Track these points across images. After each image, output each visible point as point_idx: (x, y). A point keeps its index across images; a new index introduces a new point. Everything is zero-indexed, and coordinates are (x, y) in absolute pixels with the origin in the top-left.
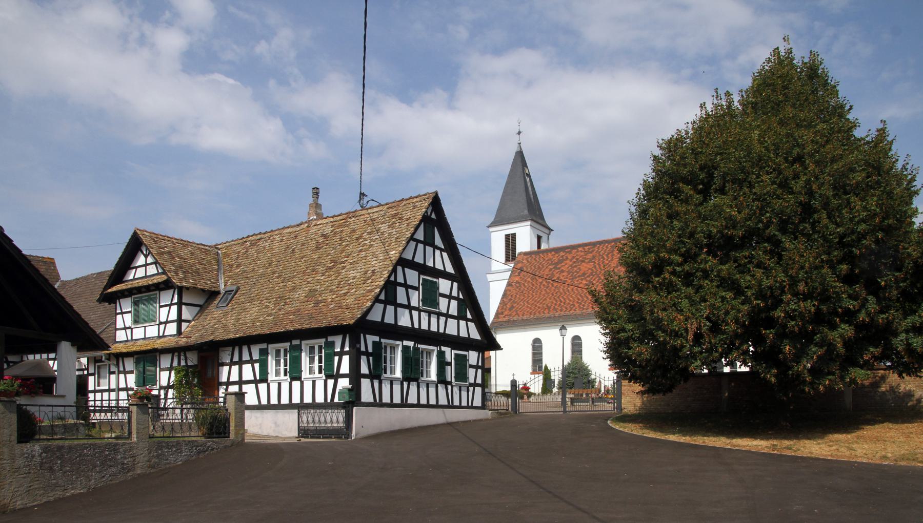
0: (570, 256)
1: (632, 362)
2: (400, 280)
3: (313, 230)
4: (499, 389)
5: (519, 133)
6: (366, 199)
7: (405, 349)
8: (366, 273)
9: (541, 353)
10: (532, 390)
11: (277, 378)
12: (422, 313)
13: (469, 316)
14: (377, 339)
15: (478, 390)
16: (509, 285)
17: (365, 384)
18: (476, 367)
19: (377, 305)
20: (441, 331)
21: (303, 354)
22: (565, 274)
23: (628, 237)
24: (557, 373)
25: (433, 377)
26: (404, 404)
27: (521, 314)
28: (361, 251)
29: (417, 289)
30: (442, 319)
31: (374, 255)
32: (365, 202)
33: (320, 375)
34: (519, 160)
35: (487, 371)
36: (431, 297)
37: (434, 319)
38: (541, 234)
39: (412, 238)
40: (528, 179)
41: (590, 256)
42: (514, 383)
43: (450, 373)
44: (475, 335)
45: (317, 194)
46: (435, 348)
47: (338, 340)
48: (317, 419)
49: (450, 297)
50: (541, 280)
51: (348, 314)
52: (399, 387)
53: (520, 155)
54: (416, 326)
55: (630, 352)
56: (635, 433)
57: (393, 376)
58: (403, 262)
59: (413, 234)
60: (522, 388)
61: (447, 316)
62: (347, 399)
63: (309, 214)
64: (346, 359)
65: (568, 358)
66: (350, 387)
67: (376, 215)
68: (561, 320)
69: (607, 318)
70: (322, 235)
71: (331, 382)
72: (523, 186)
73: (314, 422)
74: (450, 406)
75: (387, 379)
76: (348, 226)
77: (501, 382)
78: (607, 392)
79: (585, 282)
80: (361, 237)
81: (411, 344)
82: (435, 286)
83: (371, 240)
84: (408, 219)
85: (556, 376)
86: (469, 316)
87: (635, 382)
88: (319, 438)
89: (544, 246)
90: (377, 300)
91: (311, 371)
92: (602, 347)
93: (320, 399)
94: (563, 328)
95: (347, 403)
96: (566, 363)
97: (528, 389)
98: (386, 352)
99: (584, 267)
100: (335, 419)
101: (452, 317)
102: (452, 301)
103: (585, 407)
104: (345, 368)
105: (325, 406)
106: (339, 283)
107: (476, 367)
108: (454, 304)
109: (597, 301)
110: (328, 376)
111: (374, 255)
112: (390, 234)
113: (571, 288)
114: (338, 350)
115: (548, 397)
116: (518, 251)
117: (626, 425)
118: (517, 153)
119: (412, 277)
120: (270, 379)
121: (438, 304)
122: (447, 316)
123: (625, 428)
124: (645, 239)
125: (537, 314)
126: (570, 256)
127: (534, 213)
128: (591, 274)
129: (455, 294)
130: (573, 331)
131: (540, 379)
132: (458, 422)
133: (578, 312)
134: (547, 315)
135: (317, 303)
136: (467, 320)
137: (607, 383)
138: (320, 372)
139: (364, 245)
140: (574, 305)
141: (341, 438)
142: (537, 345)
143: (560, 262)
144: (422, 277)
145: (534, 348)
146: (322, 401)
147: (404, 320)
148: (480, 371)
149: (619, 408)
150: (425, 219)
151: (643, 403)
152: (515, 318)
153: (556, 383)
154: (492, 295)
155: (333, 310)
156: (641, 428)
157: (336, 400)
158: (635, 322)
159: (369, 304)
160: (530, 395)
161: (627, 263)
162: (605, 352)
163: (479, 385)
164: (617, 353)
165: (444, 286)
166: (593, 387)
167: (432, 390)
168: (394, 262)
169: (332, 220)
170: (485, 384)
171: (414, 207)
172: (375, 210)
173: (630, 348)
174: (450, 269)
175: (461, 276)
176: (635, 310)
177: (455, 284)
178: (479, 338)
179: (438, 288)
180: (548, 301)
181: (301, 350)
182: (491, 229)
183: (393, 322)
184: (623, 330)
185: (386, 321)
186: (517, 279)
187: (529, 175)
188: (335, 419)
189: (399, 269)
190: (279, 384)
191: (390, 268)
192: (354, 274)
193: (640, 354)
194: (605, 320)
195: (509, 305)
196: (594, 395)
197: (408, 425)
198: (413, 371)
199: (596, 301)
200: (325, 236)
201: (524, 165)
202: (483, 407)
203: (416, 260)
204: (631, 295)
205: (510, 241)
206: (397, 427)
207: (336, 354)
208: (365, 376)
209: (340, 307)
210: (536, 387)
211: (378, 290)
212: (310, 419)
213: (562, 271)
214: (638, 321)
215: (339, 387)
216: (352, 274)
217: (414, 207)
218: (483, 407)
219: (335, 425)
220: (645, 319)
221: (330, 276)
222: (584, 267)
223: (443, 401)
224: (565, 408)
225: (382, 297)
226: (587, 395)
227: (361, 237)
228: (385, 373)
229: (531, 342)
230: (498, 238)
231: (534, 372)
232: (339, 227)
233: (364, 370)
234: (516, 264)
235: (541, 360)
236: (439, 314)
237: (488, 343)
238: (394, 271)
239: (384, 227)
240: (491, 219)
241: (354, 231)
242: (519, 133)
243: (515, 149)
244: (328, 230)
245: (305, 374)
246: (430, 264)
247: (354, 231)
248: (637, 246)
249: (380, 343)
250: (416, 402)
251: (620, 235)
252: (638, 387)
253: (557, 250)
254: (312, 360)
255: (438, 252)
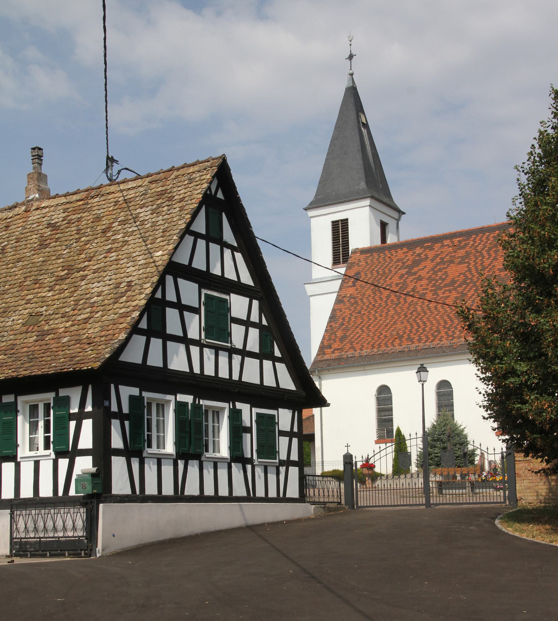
0: (431, 254)
1: (529, 424)
2: (171, 296)
3: (35, 216)
4: (328, 468)
5: (351, 57)
6: (116, 168)
7: (180, 407)
8: (118, 286)
9: (391, 410)
10: (377, 470)
11: (33, 453)
12: (206, 350)
13: (277, 353)
14: (135, 391)
15: (294, 471)
16: (339, 301)
17: (118, 465)
18: (290, 434)
19: (135, 337)
20: (235, 377)
21: (20, 418)
23: (516, 222)
24: (414, 442)
25: (224, 452)
26: (179, 497)
27: (358, 347)
28: (109, 251)
29: (196, 311)
30: (237, 359)
31: (129, 257)
32: (115, 172)
33: (47, 452)
34: (352, 100)
35: (306, 440)
36: (218, 323)
37: (223, 359)
38: (386, 219)
39: (188, 231)
40: (364, 131)
41: (461, 253)
42: (348, 459)
43: (250, 444)
44: (287, 383)
45: (40, 157)
46: (225, 405)
47: (74, 395)
48: (41, 524)
49: (247, 323)
50: (388, 292)
51: (90, 352)
52: (171, 468)
53: (352, 93)
54: (197, 370)
55: (525, 408)
56: (538, 540)
57: (162, 451)
58: (175, 269)
59: (189, 224)
60: (363, 466)
61: (244, 353)
62: (89, 490)
63: (27, 190)
64: (87, 425)
65: (431, 418)
66: (94, 470)
67: (131, 194)
68: (418, 353)
69: (487, 354)
70: (49, 225)
71: (64, 463)
72: (358, 142)
73: (36, 529)
74: (251, 498)
75: (152, 456)
76: (89, 210)
77: (329, 457)
78: (494, 471)
79: (454, 294)
80: (109, 229)
81: (188, 399)
82: (225, 306)
83: (126, 234)
84: (181, 200)
85: (415, 448)
86: (277, 353)
87: (535, 456)
88: (44, 556)
89: (391, 239)
90: (135, 330)
91: (33, 446)
92: (481, 400)
93: (46, 491)
94: (422, 369)
95: (89, 497)
96: (428, 425)
97: (372, 467)
98: (150, 413)
99: (454, 271)
100: (69, 524)
101: (252, 355)
102: (251, 329)
103: (459, 497)
104: (86, 441)
105: (57, 502)
106: (77, 302)
107: (290, 434)
108: (254, 333)
109: (471, 327)
110: (60, 454)
111: (129, 257)
112: (154, 224)
113: (432, 305)
114: (74, 410)
115: (403, 481)
116: (353, 245)
117: (524, 526)
118: (347, 89)
119: (190, 292)
120: (20, 455)
121: (230, 335)
122: (244, 353)
123: (522, 531)
124: (543, 227)
125: (383, 348)
126: (431, 254)
127: (376, 187)
128: (464, 282)
129: (255, 318)
130: (437, 373)
131: (390, 450)
132: (263, 525)
133: (445, 342)
134: (398, 348)
135: (42, 335)
136: (275, 360)
137: (491, 458)
138: (47, 447)
139: (114, 242)
140: (438, 331)
141: (79, 555)
142: (384, 396)
143: (416, 263)
144: (204, 291)
146: (50, 494)
147: (178, 362)
148: (295, 441)
149: (513, 498)
150: (208, 200)
151: (550, 490)
152: (350, 353)
153: (414, 458)
154: (313, 314)
155: (67, 346)
156: (548, 533)
157: (72, 492)
158: (530, 359)
159: (123, 336)
160: (375, 477)
161: (516, 266)
162: (487, 408)
163: (294, 464)
164: (504, 408)
165: (239, 305)
166: (472, 462)
167: (223, 473)
168: (161, 268)
169: (63, 200)
170: (305, 460)
171: (191, 181)
172: (131, 185)
173: (524, 402)
174: (246, 279)
175: (263, 290)
176: (529, 338)
177: (255, 303)
178: (292, 387)
179: (229, 310)
180: (399, 326)
181: (17, 411)
182: (311, 213)
183: (161, 365)
184: (513, 372)
185: (150, 363)
186: (352, 291)
187: (366, 126)
188: (69, 524)
189: (169, 279)
190: (37, 464)
191: (155, 279)
192: (99, 288)
193: (540, 412)
194: (481, 356)
195: (339, 334)
196: (472, 477)
197: (185, 531)
198: (192, 443)
199: (470, 326)
200: (53, 226)
201: (359, 109)
202: (302, 498)
203: (194, 265)
204: (523, 317)
205: (340, 230)
206: (168, 535)
207: (71, 417)
208: (118, 452)
209: (79, 341)
210: (384, 464)
211: (136, 314)
212: (31, 525)
213: (420, 279)
214: (535, 358)
215: (77, 471)
216: (96, 287)
217: (191, 181)
218: (302, 498)
219: (70, 534)
220: (546, 355)
221: (62, 291)
222: (454, 271)
223: (240, 490)
224: (428, 498)
225: (143, 325)
226: (463, 476)
227: (109, 229)
228: (150, 446)
229: (374, 392)
231: (380, 439)
232: (75, 211)
233: (117, 442)
234: (348, 268)
235: (391, 420)
236: (232, 351)
237: (308, 397)
238: (161, 282)
239: (144, 213)
240: (310, 195)
241: (98, 219)
242: (351, 57)
243: (345, 84)
244: (58, 217)
245: (23, 451)
246: (216, 271)
247: (98, 219)
248: (531, 238)
249: (140, 399)
250: (197, 493)
251: (505, 220)
252: (538, 464)
253: (411, 245)
254: (34, 428)
255: (227, 253)
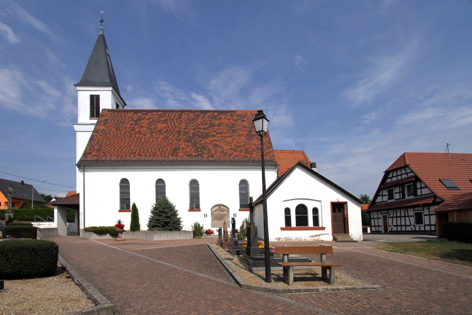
0: (147, 117)
9: (129, 193)
22: (145, 129)
40: (109, 58)
41: (163, 119)
128: (166, 132)
143: (139, 120)
145: (121, 187)
180: (132, 147)
182: (78, 88)
186: (103, 127)
195: (96, 147)
205: (95, 100)
213: (142, 127)
229: (119, 182)
230: (84, 96)
